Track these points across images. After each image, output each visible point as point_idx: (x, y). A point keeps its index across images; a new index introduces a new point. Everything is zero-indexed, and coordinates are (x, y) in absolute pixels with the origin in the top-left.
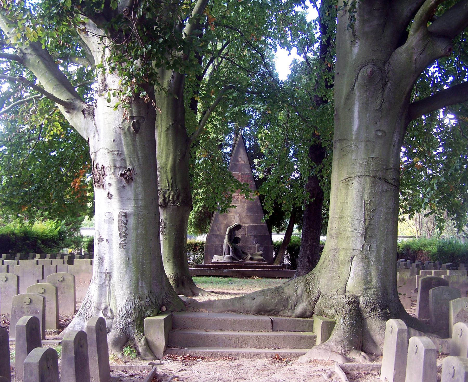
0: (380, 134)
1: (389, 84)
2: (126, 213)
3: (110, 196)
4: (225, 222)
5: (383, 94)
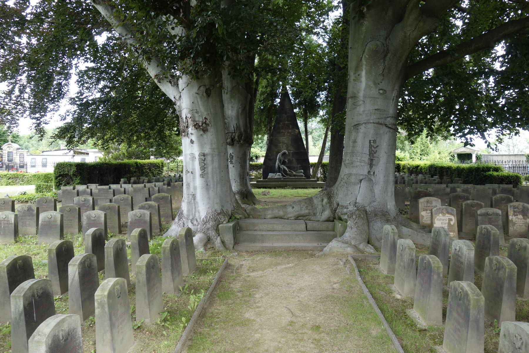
0: (381, 92)
1: (389, 55)
2: (204, 153)
3: (192, 142)
4: (276, 150)
5: (384, 63)
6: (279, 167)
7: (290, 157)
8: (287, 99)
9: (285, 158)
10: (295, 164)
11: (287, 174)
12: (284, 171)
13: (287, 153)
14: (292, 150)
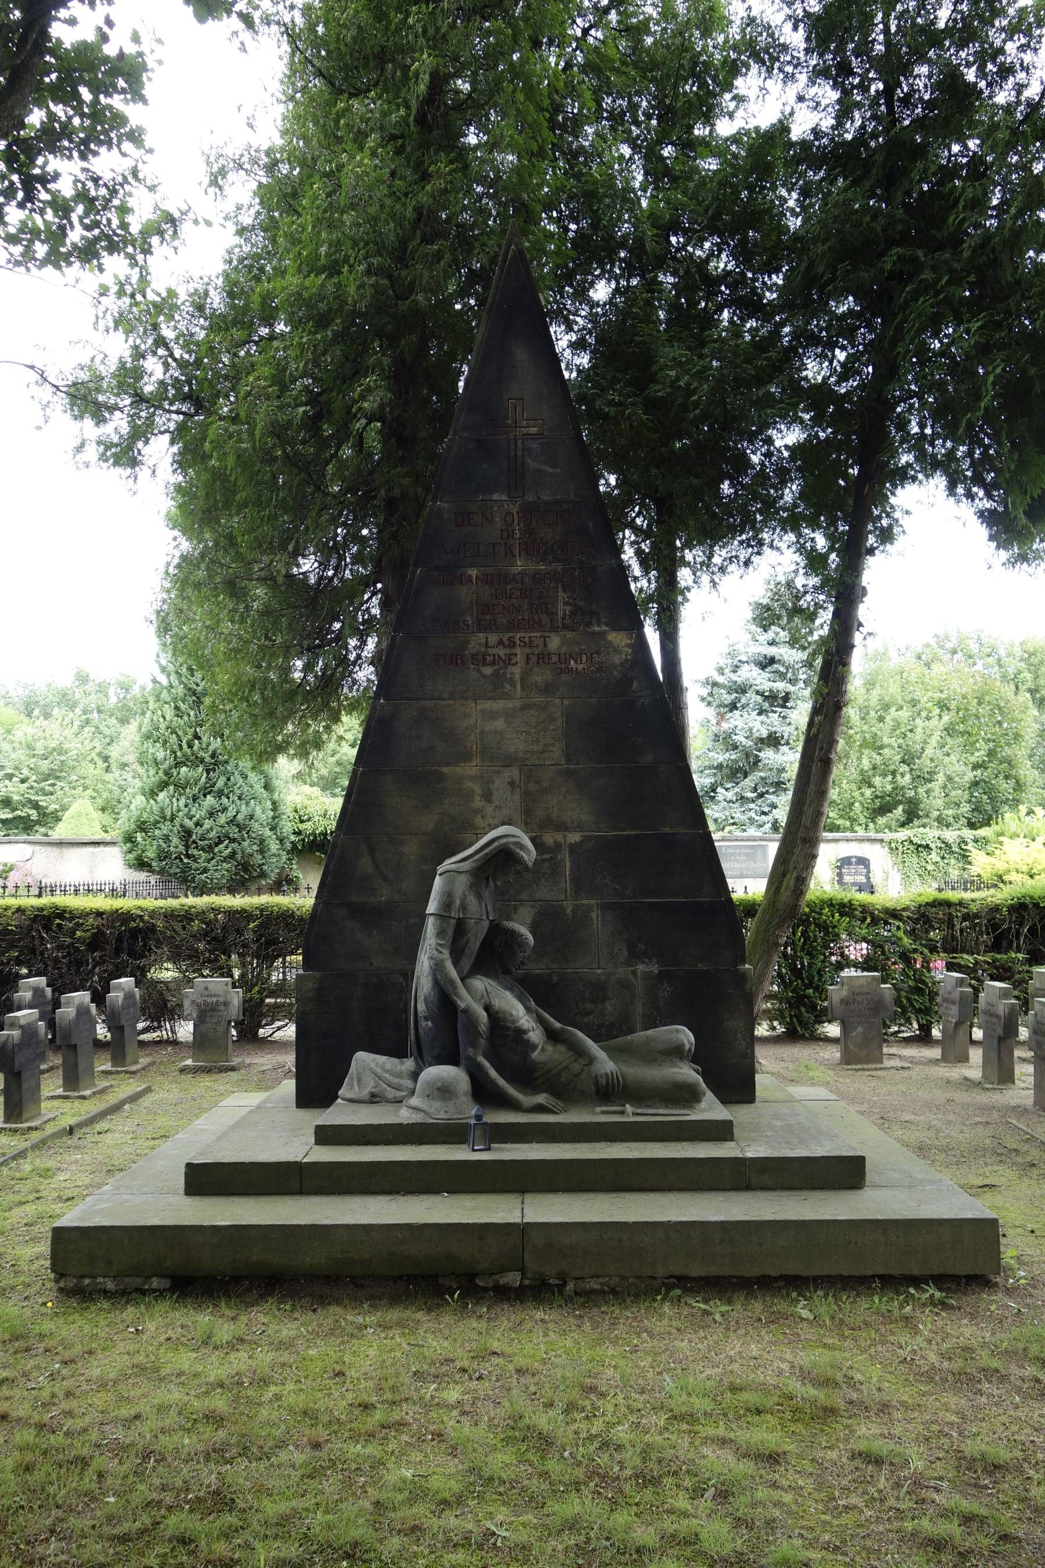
4: (428, 822)
6: (444, 1000)
7: (560, 892)
8: (522, 355)
9: (506, 906)
10: (605, 959)
11: (528, 1076)
12: (502, 1033)
13: (530, 854)
14: (577, 818)
